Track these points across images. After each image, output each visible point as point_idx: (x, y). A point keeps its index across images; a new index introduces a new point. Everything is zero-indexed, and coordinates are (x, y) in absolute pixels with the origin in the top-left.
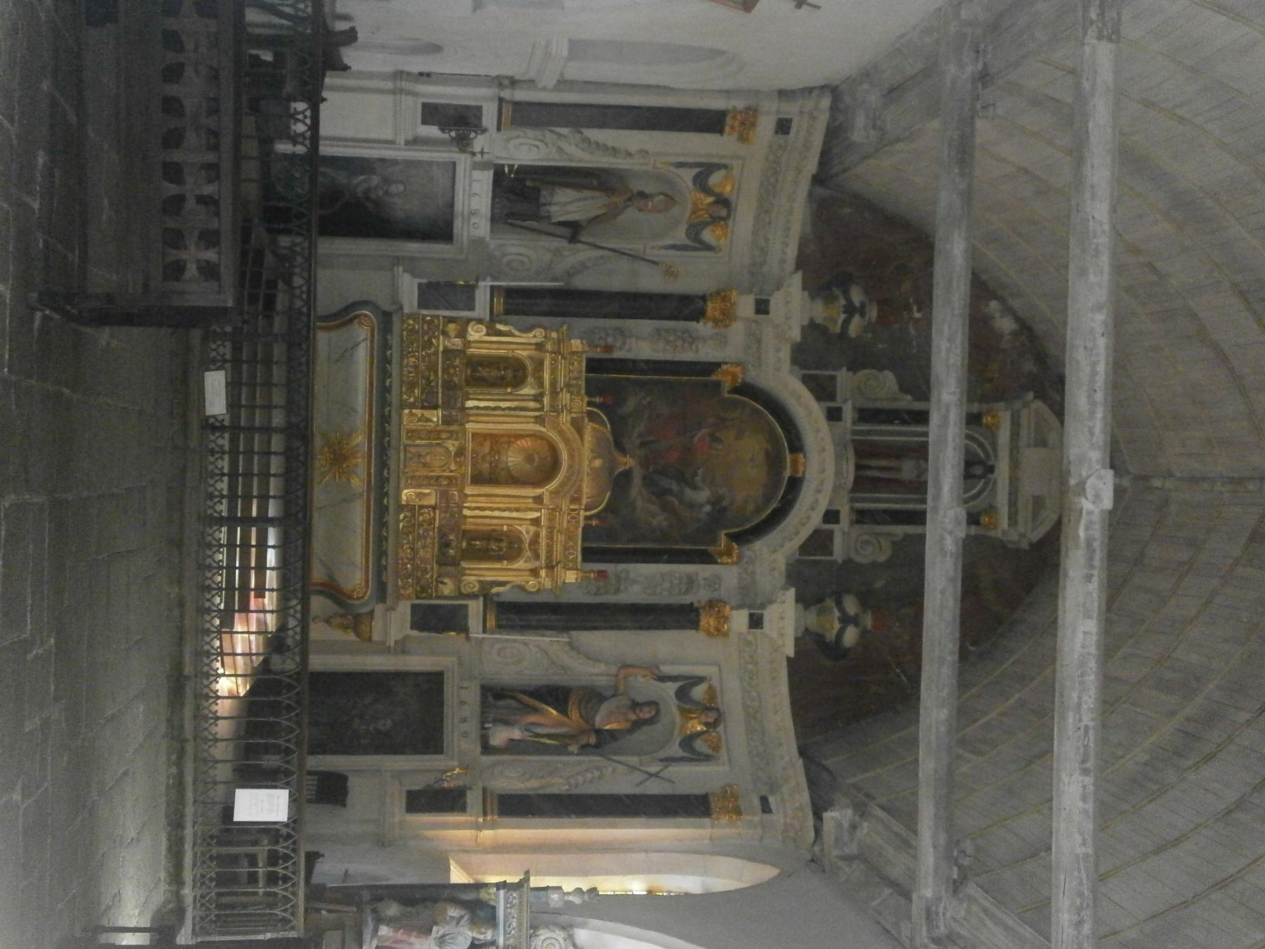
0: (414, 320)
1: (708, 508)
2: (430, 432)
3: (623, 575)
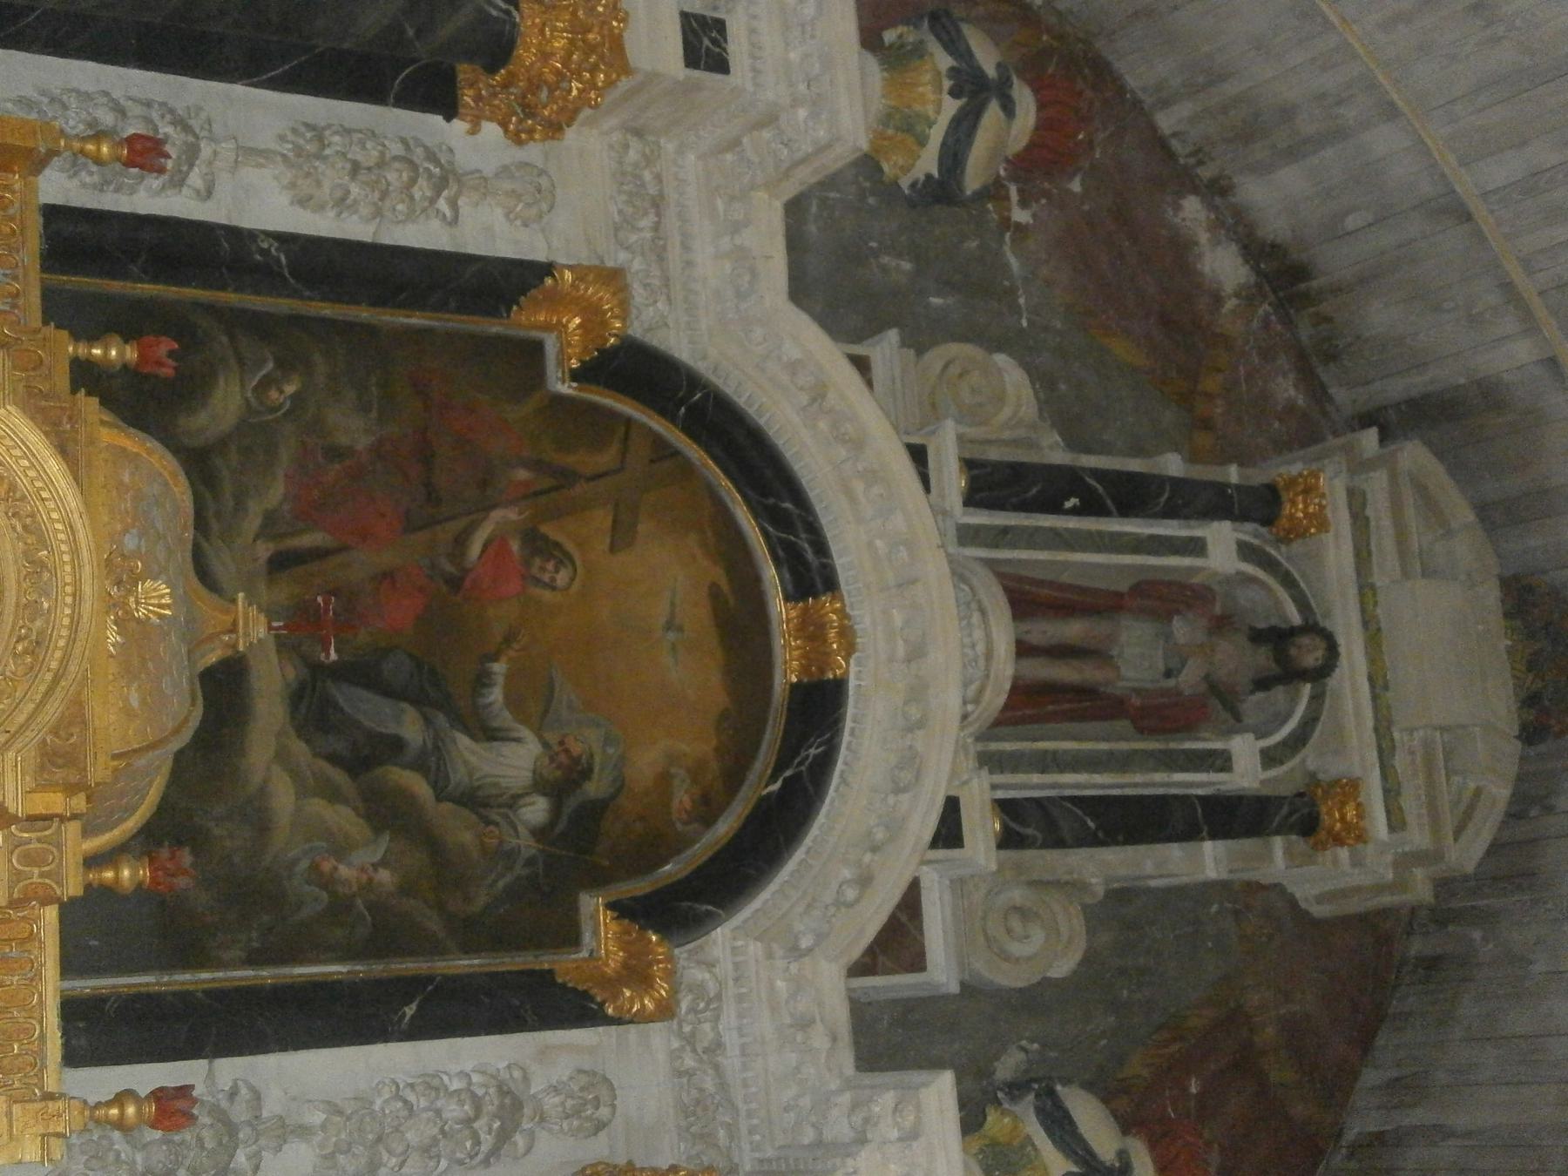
1: (536, 810)
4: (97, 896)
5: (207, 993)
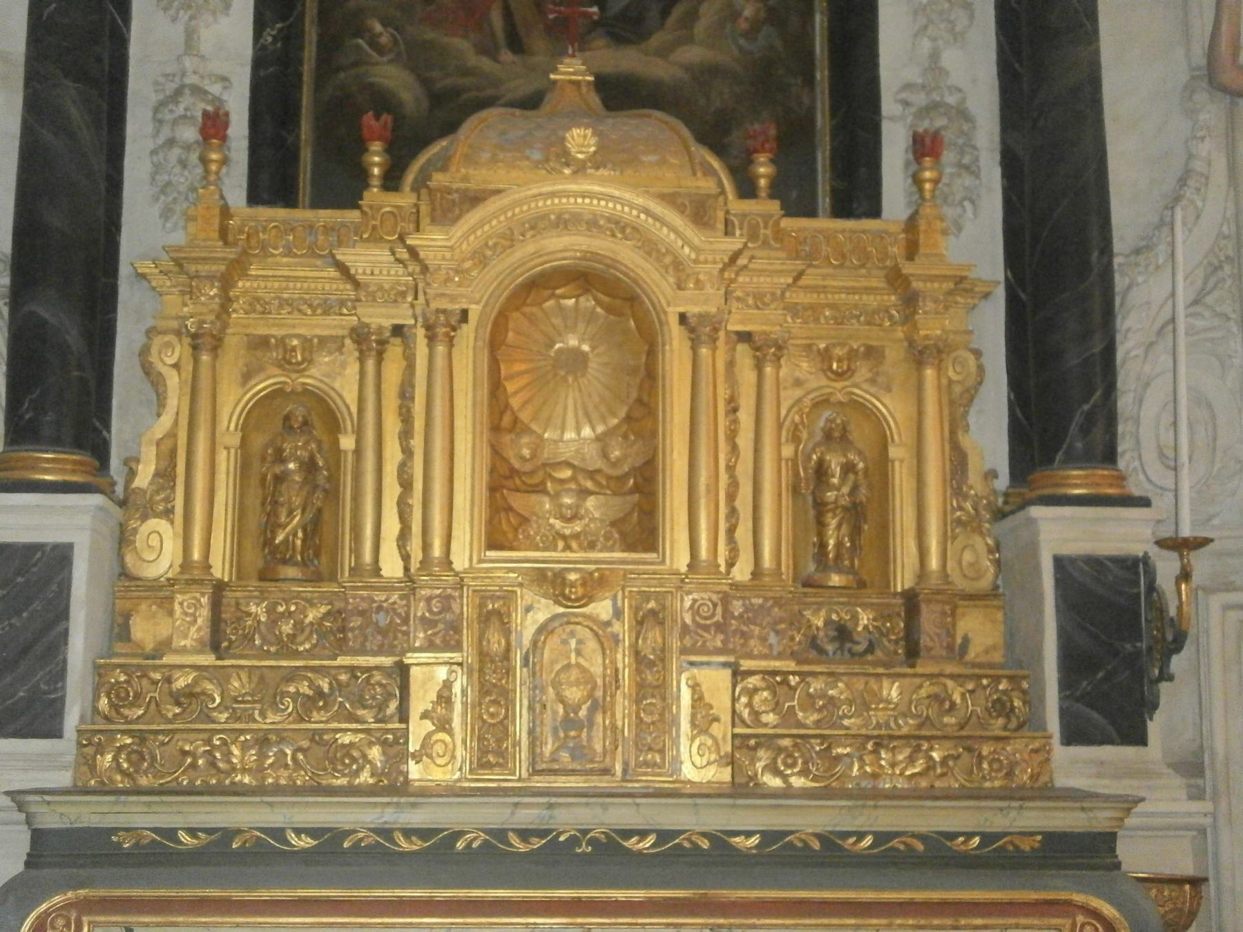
0: (100, 749)
2: (484, 690)
3: (920, 99)
4: (777, 190)
5: (833, 116)
